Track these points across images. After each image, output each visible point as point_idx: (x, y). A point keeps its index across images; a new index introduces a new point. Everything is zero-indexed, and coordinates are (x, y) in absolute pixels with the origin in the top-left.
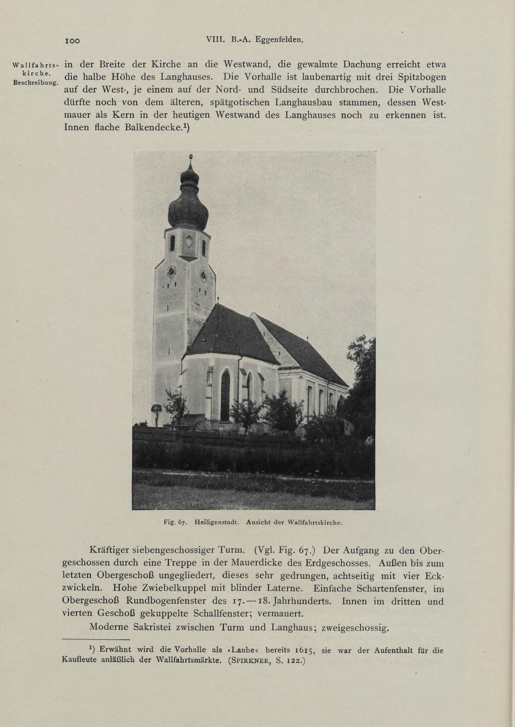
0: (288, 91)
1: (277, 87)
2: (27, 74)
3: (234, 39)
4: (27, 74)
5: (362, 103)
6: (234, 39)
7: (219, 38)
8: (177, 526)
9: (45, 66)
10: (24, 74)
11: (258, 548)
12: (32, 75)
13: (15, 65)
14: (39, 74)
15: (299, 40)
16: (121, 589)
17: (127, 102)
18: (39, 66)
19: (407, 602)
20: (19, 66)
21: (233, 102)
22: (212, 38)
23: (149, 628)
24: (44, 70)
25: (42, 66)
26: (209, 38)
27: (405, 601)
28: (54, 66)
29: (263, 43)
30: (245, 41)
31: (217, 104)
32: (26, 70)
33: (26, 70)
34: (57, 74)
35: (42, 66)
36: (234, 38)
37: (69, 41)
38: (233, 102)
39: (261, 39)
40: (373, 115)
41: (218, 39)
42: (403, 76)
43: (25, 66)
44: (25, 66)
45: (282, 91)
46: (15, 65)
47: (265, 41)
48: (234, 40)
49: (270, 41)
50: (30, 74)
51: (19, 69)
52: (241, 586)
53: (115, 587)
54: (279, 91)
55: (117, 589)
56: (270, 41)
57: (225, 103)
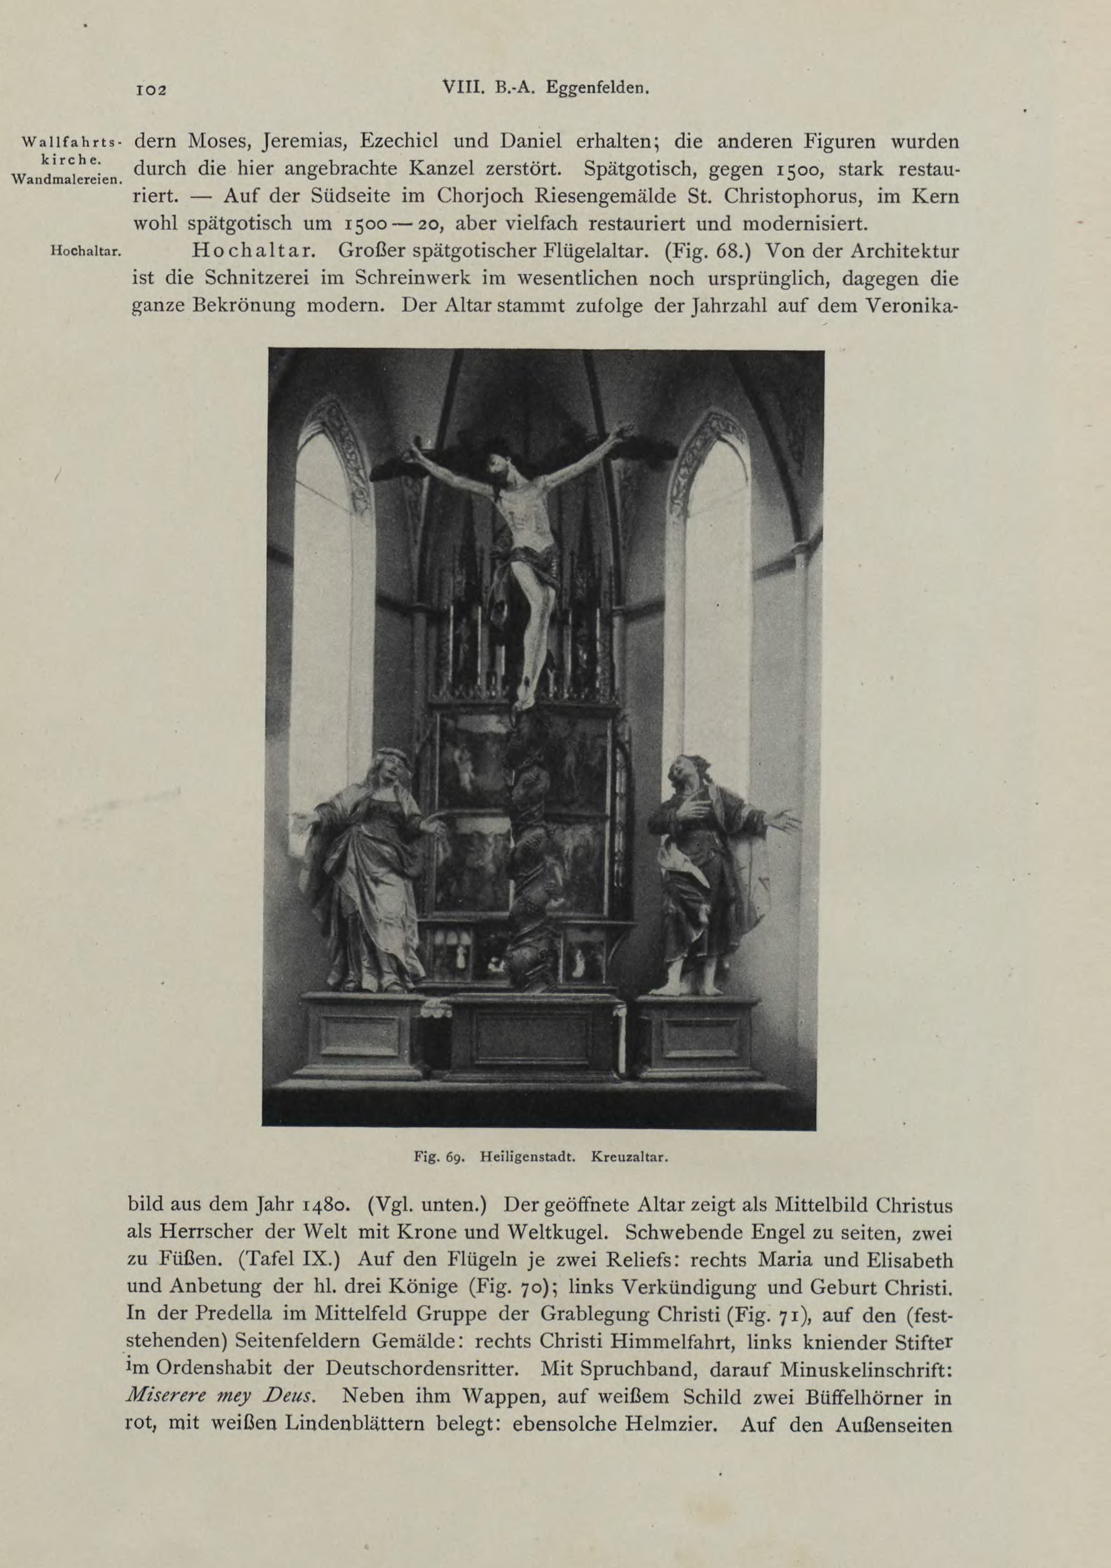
0: (347, 198)
1: (323, 191)
2: (50, 161)
3: (501, 86)
4: (50, 161)
5: (546, 306)
6: (501, 86)
7: (473, 84)
8: (442, 1165)
9: (92, 144)
10: (45, 162)
11: (376, 1200)
12: (62, 163)
13: (29, 142)
14: (77, 160)
15: (639, 89)
16: (177, 1234)
17: (148, 223)
18: (80, 142)
19: (347, 1315)
20: (37, 143)
21: (236, 224)
22: (457, 84)
23: (228, 306)
24: (87, 153)
25: (86, 143)
26: (449, 84)
27: (343, 1311)
28: (112, 143)
29: (562, 94)
30: (523, 90)
31: (203, 226)
32: (49, 152)
33: (49, 152)
34: (119, 161)
35: (86, 143)
36: (501, 84)
37: (143, 90)
38: (236, 224)
39: (557, 86)
40: (585, 306)
41: (473, 86)
42: (595, 166)
43: (48, 143)
44: (48, 143)
45: (334, 198)
46: (29, 142)
47: (567, 91)
48: (502, 89)
49: (577, 91)
50: (58, 161)
51: (36, 151)
52: (873, 1366)
53: (164, 1230)
54: (329, 199)
55: (168, 1234)
56: (577, 91)
57: (218, 224)
